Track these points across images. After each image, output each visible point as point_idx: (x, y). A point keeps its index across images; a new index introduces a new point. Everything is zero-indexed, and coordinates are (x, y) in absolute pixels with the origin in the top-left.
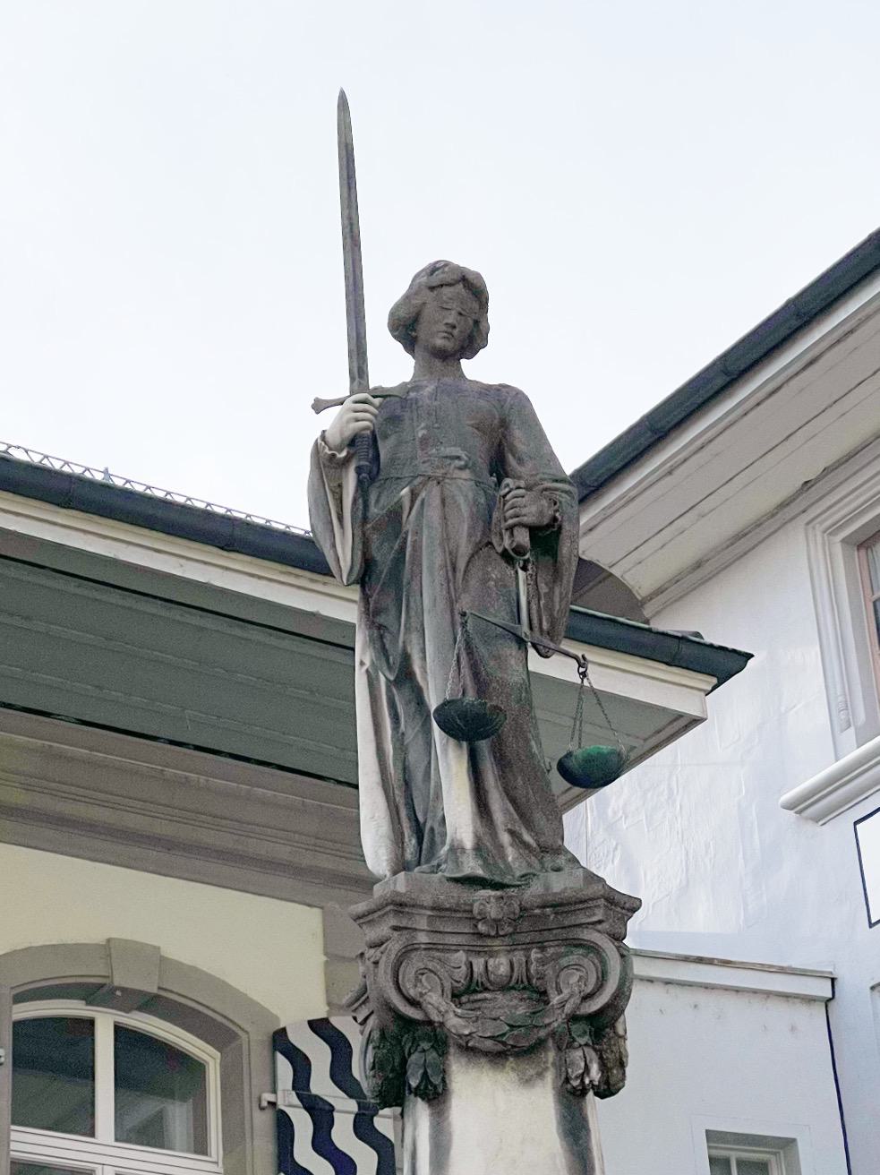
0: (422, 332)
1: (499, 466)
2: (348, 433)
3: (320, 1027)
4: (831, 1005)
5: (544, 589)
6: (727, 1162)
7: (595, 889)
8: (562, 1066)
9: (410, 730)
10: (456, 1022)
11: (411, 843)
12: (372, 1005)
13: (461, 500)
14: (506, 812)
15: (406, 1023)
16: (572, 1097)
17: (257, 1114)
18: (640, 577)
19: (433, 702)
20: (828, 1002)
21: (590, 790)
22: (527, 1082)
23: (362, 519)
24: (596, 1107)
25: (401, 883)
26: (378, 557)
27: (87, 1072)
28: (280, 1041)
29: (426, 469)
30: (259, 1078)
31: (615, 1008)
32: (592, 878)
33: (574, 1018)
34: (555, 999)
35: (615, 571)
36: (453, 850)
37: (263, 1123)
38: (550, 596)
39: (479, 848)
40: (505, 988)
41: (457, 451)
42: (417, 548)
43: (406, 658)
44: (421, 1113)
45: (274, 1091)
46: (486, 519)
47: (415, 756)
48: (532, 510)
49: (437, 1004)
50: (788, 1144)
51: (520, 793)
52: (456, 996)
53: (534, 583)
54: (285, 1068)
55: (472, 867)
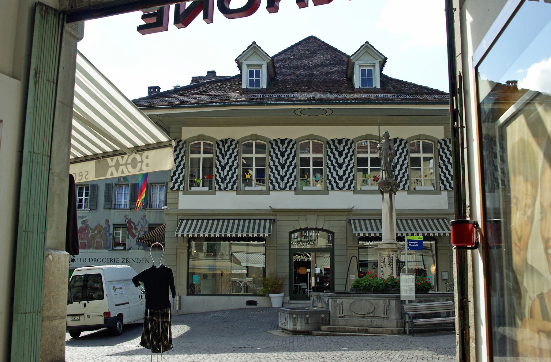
37: (437, 150)
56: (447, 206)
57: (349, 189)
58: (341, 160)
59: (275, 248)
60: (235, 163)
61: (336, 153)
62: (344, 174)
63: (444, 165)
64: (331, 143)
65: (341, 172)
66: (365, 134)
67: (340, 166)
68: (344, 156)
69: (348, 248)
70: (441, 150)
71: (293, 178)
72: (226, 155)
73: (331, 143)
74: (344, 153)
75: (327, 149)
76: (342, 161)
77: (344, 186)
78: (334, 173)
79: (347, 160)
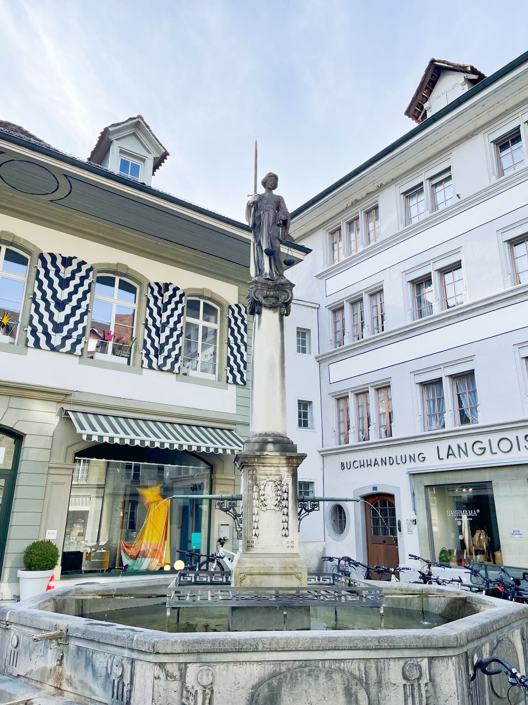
0: (267, 185)
1: (278, 209)
2: (253, 201)
3: (237, 305)
4: (319, 309)
5: (284, 231)
6: (299, 332)
7: (289, 282)
8: (280, 311)
9: (260, 254)
10: (264, 302)
11: (258, 272)
12: (250, 298)
13: (271, 214)
14: (274, 268)
15: (256, 302)
16: (281, 316)
17: (226, 318)
18: (295, 236)
19: (264, 249)
20: (318, 308)
21: (289, 266)
22: (274, 312)
23: (254, 216)
24: (285, 318)
25: (256, 278)
26: (256, 223)
27: (198, 310)
28: (230, 307)
29: (266, 208)
30: (226, 312)
31: (290, 302)
32: (288, 280)
33: (283, 303)
34: (280, 300)
35: (290, 235)
36: (265, 274)
37: (226, 320)
38: (285, 232)
39: (270, 274)
40: (272, 297)
41: (271, 206)
42: (263, 222)
43: (260, 241)
44: (257, 316)
45: (229, 315)
46: (275, 218)
47: (260, 258)
48: (283, 217)
49: (261, 298)
50: (309, 330)
51: (277, 265)
52: (264, 298)
53: (282, 229)
54: (231, 312)
55: (268, 277)
56: (235, 410)
57: (72, 352)
58: (63, 295)
59: (232, 483)
60: (84, 304)
61: (56, 281)
62: (67, 322)
63: (236, 344)
64: (49, 259)
65: (59, 317)
66: (115, 262)
67: (61, 306)
68: (71, 289)
69: (52, 471)
70: (233, 321)
71: (177, 352)
72: (165, 310)
73: (49, 259)
74: (72, 283)
75: (38, 268)
76: (66, 297)
77: (63, 345)
78: (46, 315)
79: (75, 298)
